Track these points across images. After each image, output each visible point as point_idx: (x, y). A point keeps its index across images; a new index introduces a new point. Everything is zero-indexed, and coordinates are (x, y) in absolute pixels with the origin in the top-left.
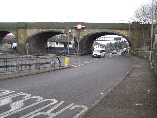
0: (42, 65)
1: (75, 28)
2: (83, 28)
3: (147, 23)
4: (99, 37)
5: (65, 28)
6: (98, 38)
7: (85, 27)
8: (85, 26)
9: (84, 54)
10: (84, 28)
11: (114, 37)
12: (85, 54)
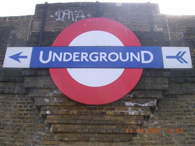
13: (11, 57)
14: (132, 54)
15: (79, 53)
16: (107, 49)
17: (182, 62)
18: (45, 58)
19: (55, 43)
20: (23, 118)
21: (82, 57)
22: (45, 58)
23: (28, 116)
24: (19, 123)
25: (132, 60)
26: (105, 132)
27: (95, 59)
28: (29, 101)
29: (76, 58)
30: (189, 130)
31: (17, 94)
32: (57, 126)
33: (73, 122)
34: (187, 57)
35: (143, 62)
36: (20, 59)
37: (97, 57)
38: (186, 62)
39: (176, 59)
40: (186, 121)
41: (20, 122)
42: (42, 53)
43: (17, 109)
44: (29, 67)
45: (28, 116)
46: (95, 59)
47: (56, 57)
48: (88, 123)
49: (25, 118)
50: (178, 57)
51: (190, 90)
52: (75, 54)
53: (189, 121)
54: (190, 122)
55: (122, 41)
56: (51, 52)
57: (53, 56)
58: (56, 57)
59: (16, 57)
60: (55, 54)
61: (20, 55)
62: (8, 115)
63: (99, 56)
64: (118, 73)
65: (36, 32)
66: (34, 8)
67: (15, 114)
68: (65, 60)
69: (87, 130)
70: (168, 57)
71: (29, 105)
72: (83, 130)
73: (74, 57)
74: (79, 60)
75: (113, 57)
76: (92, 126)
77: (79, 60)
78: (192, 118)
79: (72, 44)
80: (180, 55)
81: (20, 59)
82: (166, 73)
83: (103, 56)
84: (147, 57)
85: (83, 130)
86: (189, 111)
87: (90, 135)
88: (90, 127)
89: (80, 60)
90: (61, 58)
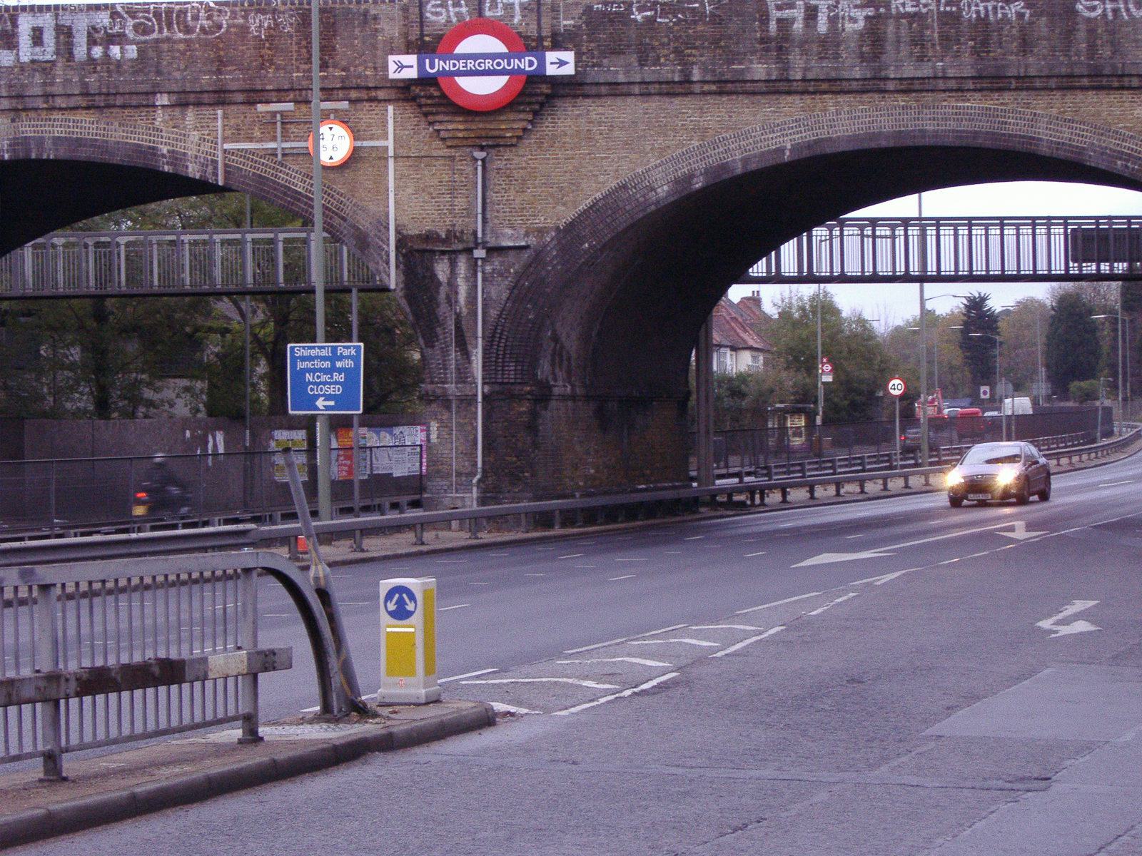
0: (87, 700)
1: (405, 91)
2: (537, 78)
3: (492, 68)
4: (798, 226)
5: (254, 96)
6: (789, 250)
7: (569, 70)
8: (569, 56)
9: (569, 518)
10: (556, 81)
11: (1065, 221)
12: (591, 516)
13: (567, 63)
14: (516, 61)
16: (493, 56)
18: (432, 67)
19: (524, 78)
21: (469, 65)
22: (432, 67)
25: (516, 67)
34: (392, 67)
35: (527, 69)
42: (427, 61)
44: (416, 77)
50: (402, 67)
52: (461, 61)
55: (458, 85)
56: (437, 60)
57: (439, 65)
59: (562, 63)
63: (484, 63)
64: (501, 81)
68: (452, 69)
70: (412, 67)
73: (460, 65)
75: (499, 64)
79: (506, 78)
83: (488, 64)
84: (531, 63)
90: (448, 66)
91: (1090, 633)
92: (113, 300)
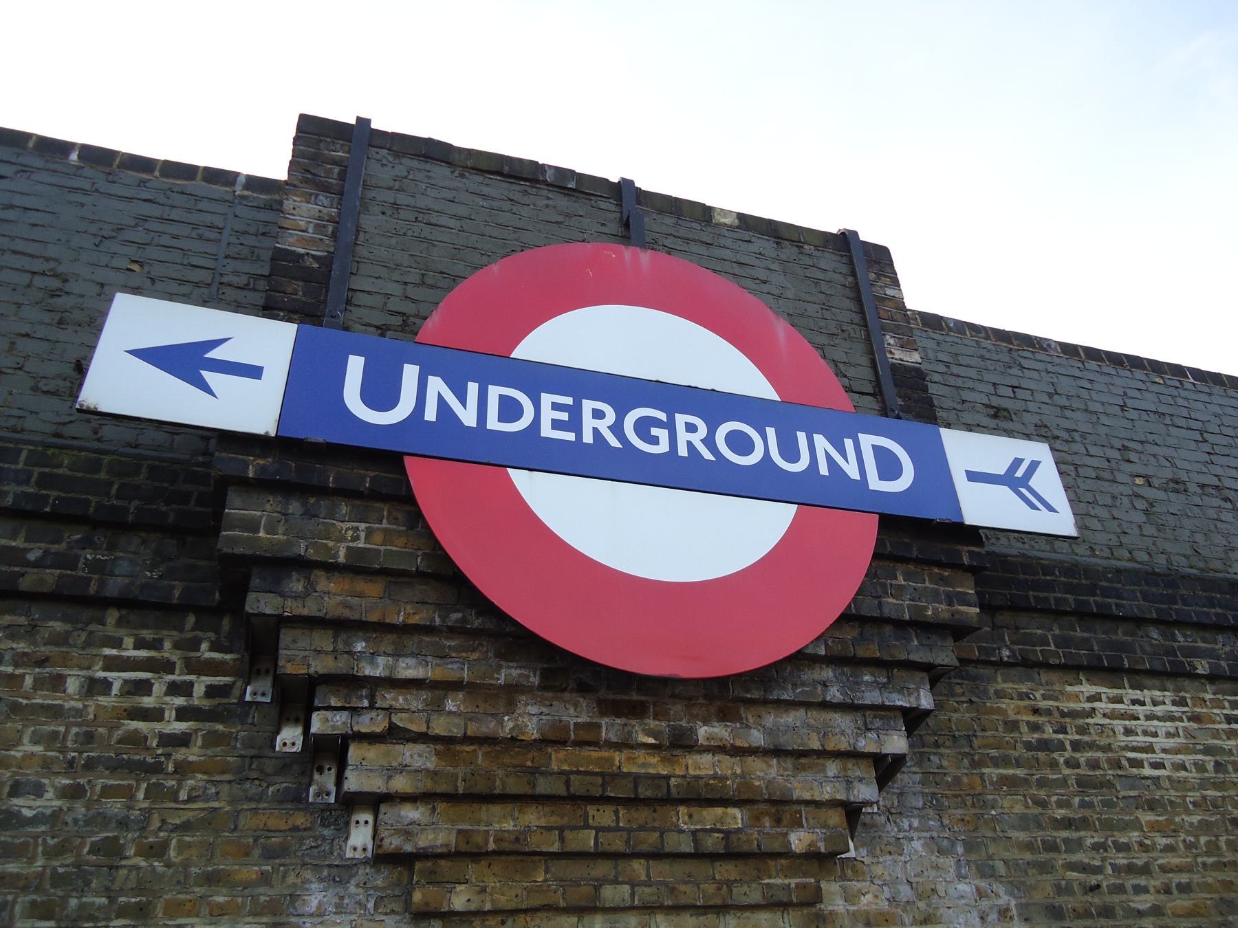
3: (614, 442)
14: (821, 442)
15: (568, 401)
17: (1034, 507)
20: (157, 768)
21: (588, 423)
23: (193, 754)
24: (115, 806)
25: (824, 470)
26: (687, 847)
27: (655, 441)
28: (209, 655)
29: (556, 424)
30: (1066, 841)
31: (124, 603)
32: (412, 813)
33: (515, 786)
35: (875, 484)
36: (208, 376)
37: (663, 434)
38: (1051, 509)
39: (1006, 488)
40: (1042, 794)
41: (129, 794)
42: (355, 366)
43: (103, 700)
45: (193, 754)
46: (655, 441)
47: (441, 400)
48: (597, 792)
49: (171, 768)
51: (1038, 649)
52: (547, 399)
53: (1055, 798)
54: (1060, 805)
58: (441, 400)
60: (436, 385)
61: (213, 354)
62: (28, 747)
63: (670, 426)
65: (302, 251)
66: (290, 131)
67: (89, 738)
68: (493, 423)
69: (587, 840)
71: (201, 685)
72: (567, 834)
74: (570, 436)
75: (740, 443)
76: (616, 812)
77: (570, 436)
78: (1064, 782)
80: (1019, 474)
81: (208, 376)
82: (966, 548)
85: (567, 834)
86: (1045, 745)
87: (602, 869)
88: (603, 816)
89: (579, 435)
91: (208, 351)
92: (569, 186)
